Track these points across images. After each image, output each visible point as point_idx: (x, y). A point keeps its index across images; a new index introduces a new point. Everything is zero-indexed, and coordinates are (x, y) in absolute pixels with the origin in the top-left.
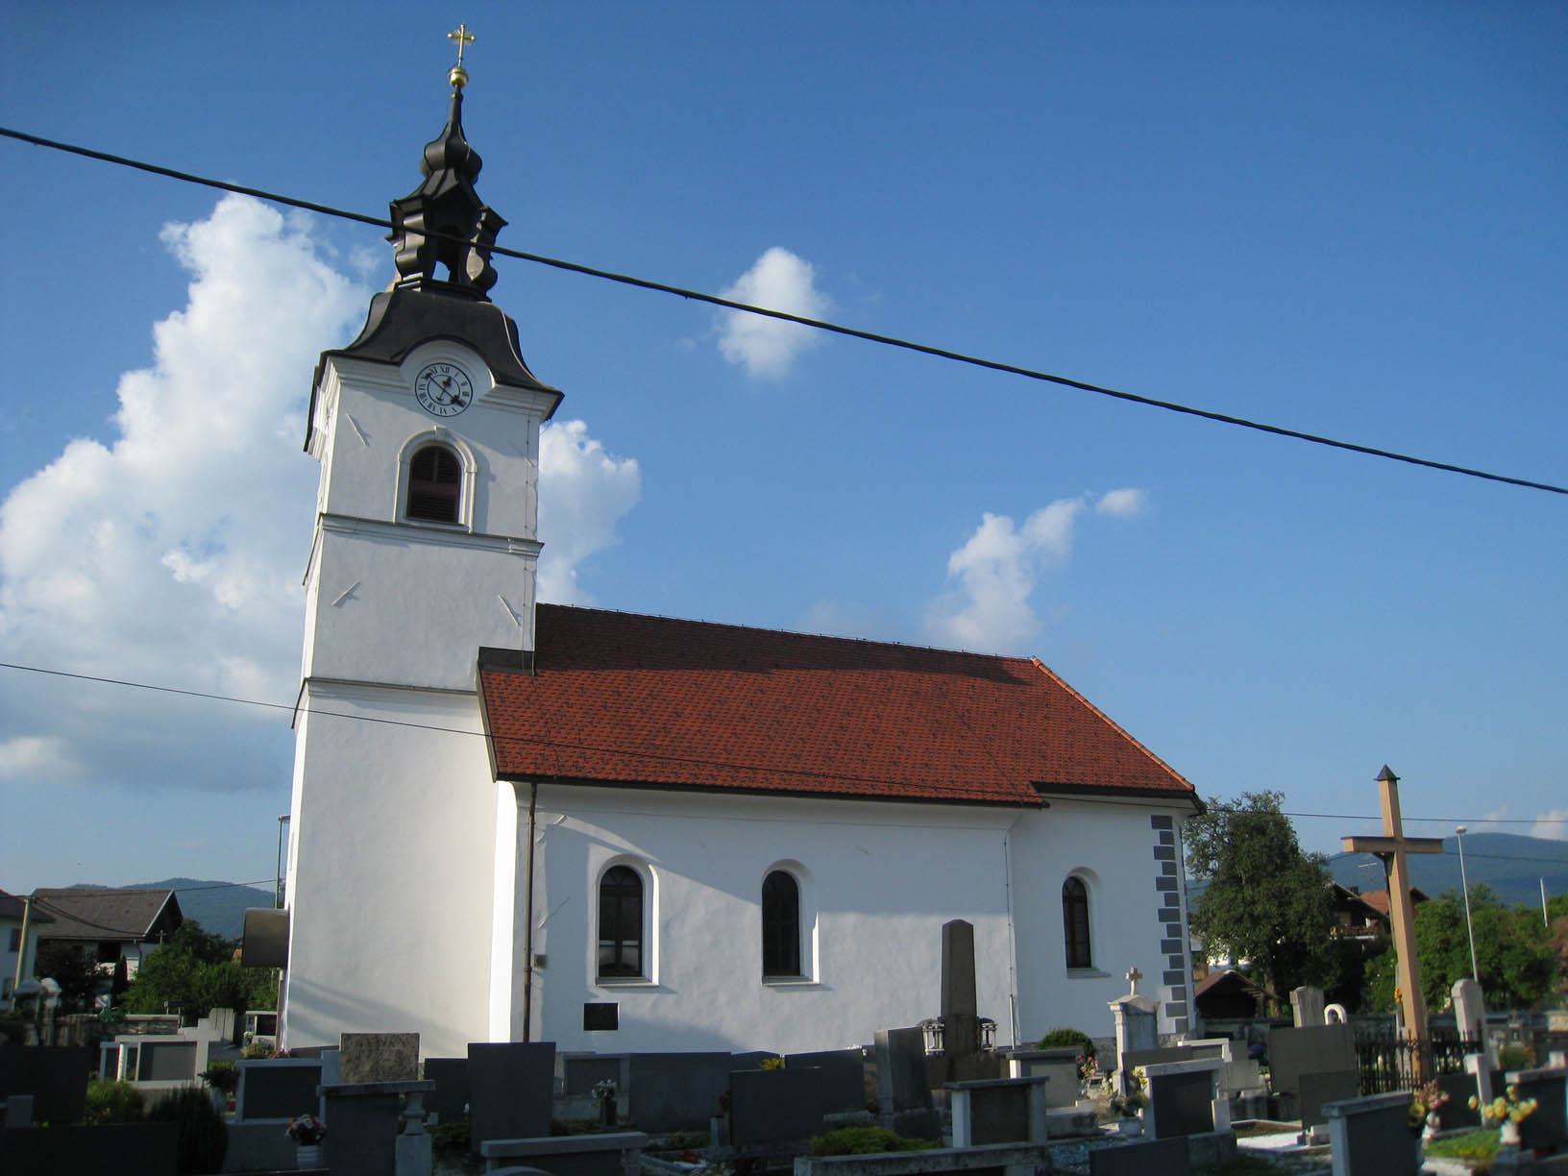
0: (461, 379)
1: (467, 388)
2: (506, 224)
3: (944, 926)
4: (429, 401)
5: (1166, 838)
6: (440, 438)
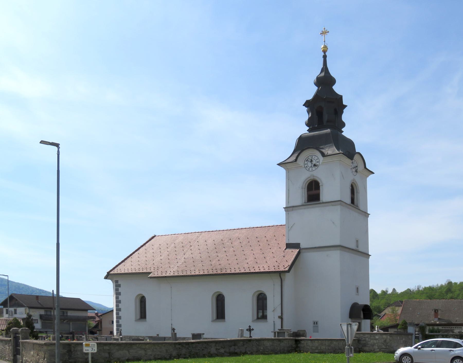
0: (316, 158)
1: (318, 160)
4: (308, 168)
6: (312, 178)
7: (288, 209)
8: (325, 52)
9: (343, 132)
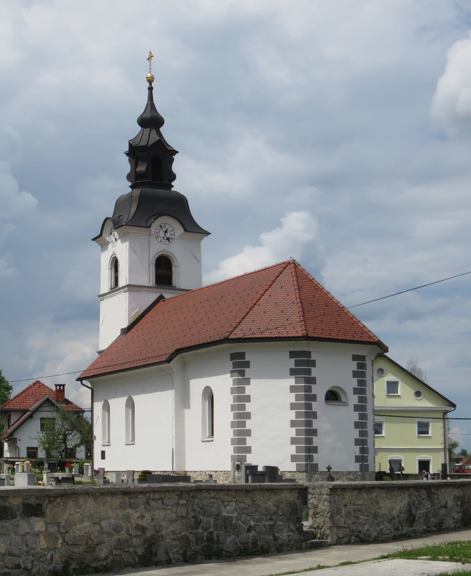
2: (177, 152)
3: (388, 398)
5: (362, 366)
7: (130, 288)
8: (150, 81)
9: (173, 186)
